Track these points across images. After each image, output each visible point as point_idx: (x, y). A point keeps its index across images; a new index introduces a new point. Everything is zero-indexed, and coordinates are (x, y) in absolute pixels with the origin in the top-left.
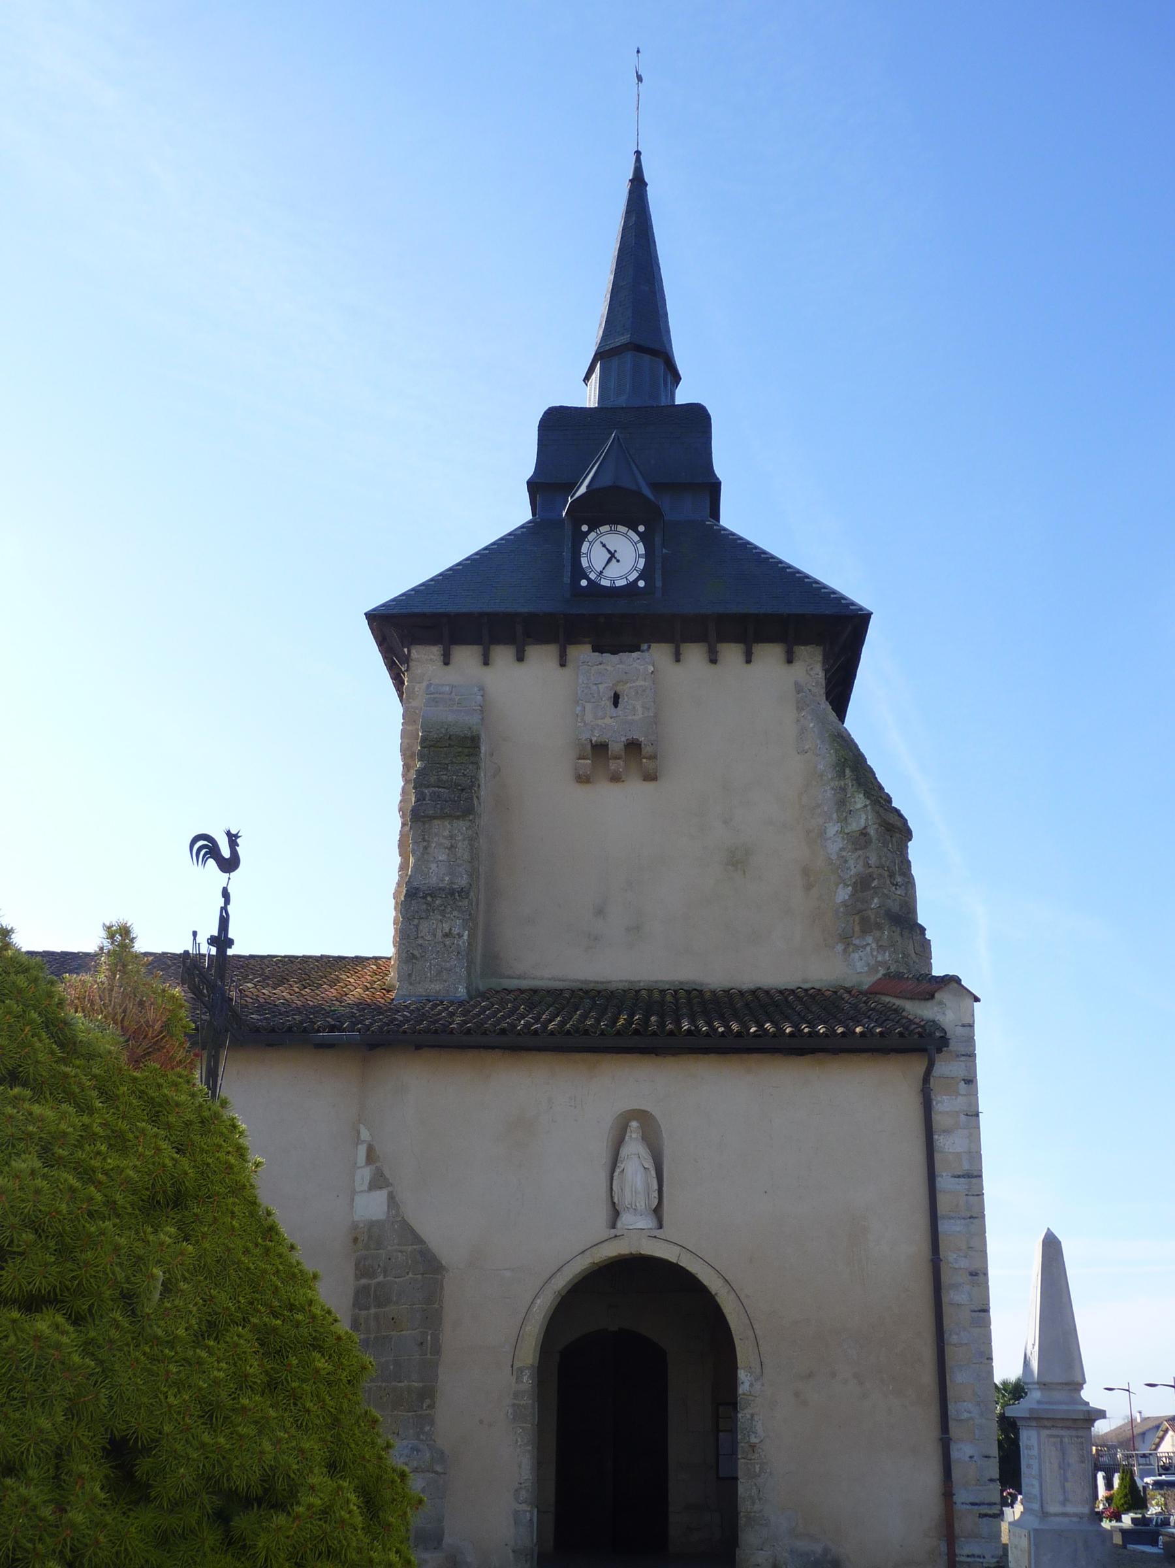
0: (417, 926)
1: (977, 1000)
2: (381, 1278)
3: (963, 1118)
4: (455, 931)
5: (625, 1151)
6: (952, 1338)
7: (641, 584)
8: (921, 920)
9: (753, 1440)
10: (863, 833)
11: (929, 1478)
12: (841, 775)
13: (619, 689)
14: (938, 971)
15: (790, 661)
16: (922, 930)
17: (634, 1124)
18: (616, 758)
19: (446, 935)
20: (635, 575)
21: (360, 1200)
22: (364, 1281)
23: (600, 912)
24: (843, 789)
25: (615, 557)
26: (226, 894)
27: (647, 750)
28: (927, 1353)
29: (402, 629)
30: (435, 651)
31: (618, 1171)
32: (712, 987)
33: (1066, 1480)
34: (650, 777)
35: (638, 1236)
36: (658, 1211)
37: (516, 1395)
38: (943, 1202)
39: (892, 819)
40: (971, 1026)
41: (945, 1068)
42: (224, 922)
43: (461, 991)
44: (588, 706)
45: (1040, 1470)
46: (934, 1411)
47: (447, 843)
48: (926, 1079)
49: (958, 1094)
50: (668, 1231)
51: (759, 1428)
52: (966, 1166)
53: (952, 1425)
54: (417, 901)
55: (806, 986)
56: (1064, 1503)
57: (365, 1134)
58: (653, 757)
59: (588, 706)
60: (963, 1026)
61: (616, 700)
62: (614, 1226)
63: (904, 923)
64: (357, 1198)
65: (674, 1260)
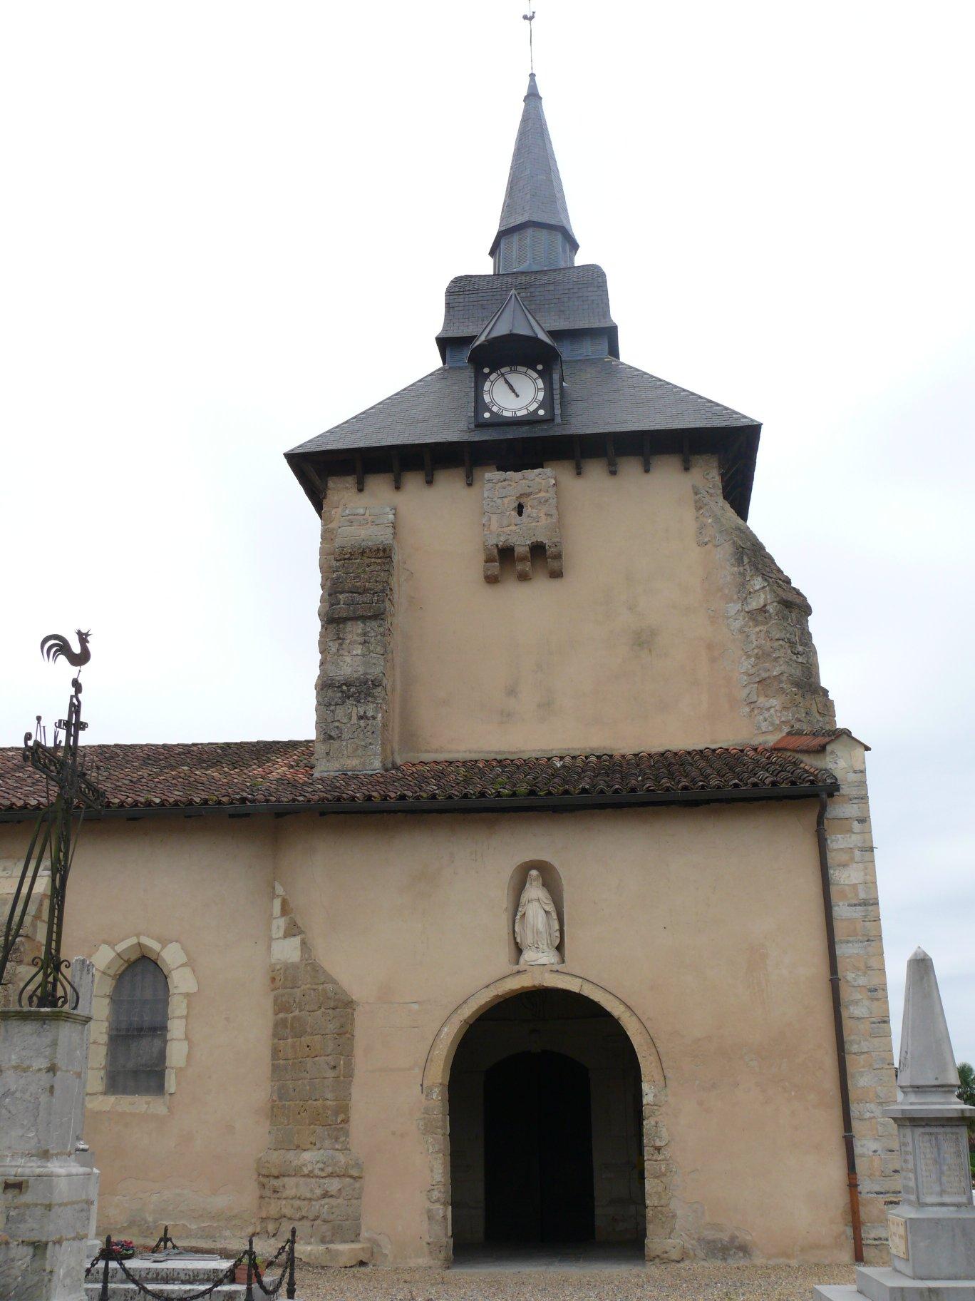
0: (333, 711)
1: (867, 749)
2: (297, 1013)
3: (857, 853)
4: (370, 714)
5: (525, 896)
6: (852, 1047)
7: (541, 412)
8: (823, 684)
9: (658, 1144)
10: (763, 610)
11: (835, 1171)
12: (740, 562)
13: (523, 500)
14: (840, 724)
15: (687, 469)
16: (825, 692)
17: (534, 873)
18: (523, 559)
19: (361, 718)
20: (535, 406)
21: (276, 946)
22: (282, 1015)
23: (512, 692)
24: (743, 575)
25: (515, 397)
26: (77, 685)
27: (551, 551)
28: (830, 1062)
29: (318, 469)
30: (350, 481)
31: (519, 914)
32: (623, 752)
33: (942, 1173)
34: (557, 574)
35: (540, 967)
36: (560, 948)
37: (427, 1111)
38: (840, 930)
39: (790, 597)
40: (863, 772)
41: (840, 810)
42: (75, 708)
43: (377, 764)
44: (494, 518)
45: (915, 1165)
46: (837, 1112)
47: (361, 639)
48: (820, 822)
49: (851, 831)
50: (572, 964)
51: (664, 1133)
52: (862, 895)
53: (855, 1124)
54: (333, 692)
55: (713, 746)
56: (942, 1192)
57: (280, 890)
58: (558, 557)
59: (494, 518)
60: (855, 772)
61: (520, 509)
62: (517, 963)
63: (807, 685)
64: (275, 945)
65: (576, 989)
